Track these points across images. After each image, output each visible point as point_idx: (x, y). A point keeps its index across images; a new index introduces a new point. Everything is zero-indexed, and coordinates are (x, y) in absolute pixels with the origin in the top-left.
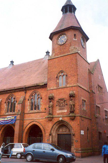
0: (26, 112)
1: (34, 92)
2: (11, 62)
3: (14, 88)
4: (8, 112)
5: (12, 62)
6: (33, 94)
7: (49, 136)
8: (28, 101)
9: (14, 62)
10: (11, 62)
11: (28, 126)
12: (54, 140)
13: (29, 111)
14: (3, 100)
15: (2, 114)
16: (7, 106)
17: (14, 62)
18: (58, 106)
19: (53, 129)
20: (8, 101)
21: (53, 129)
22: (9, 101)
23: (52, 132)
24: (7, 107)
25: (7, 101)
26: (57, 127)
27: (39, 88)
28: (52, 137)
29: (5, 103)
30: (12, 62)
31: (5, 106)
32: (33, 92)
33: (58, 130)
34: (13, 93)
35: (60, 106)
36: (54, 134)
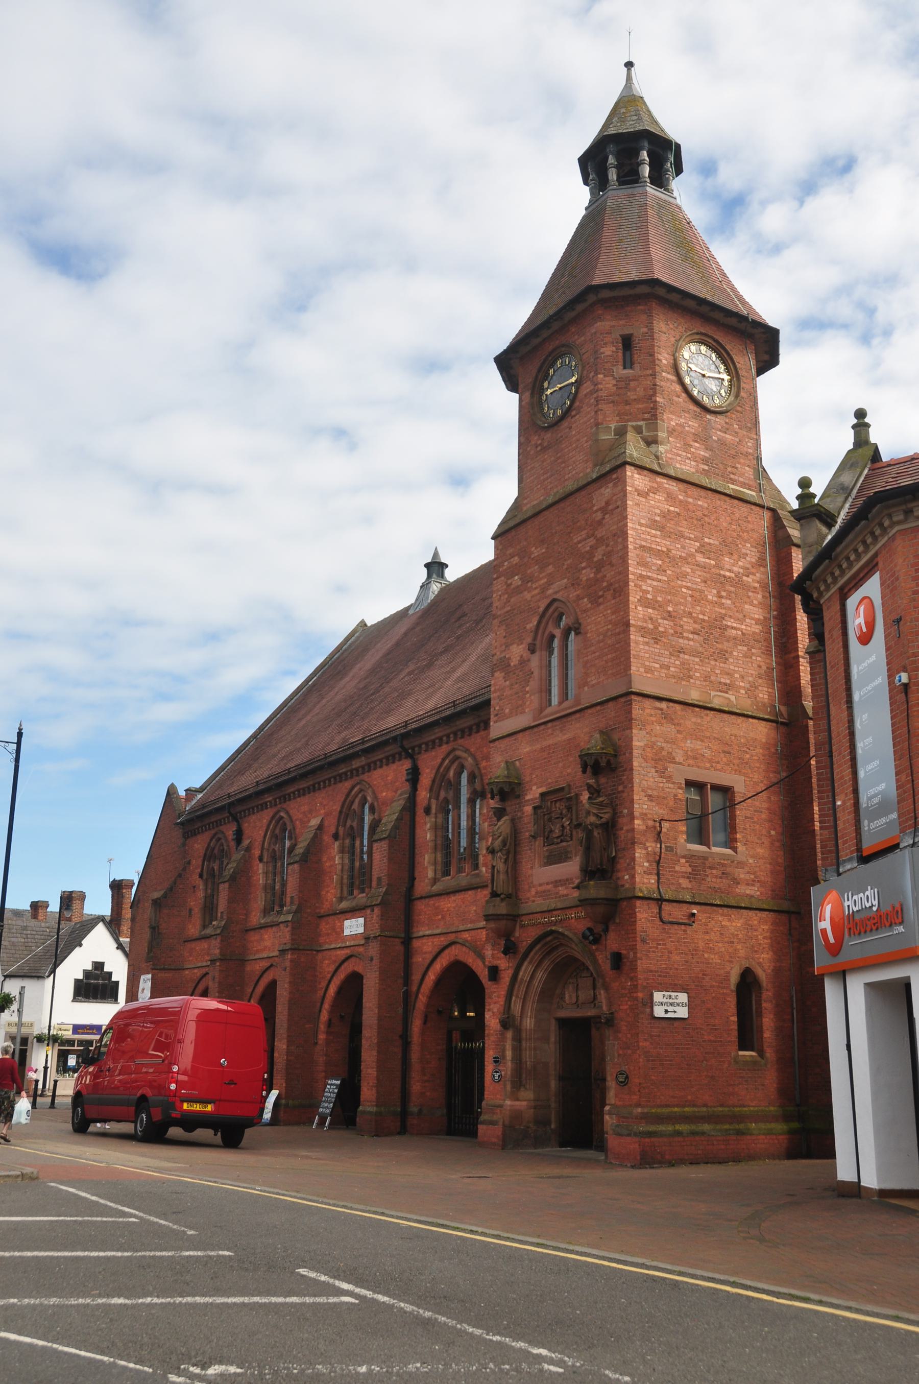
0: (422, 886)
1: (451, 757)
2: (427, 566)
3: (326, 758)
4: (446, 873)
5: (436, 568)
6: (352, 802)
7: (503, 1034)
8: (427, 819)
9: (447, 566)
10: (427, 566)
11: (432, 977)
12: (528, 1058)
13: (435, 881)
14: (326, 823)
15: (325, 907)
16: (346, 856)
17: (447, 566)
18: (540, 841)
19: (523, 988)
20: (349, 823)
21: (520, 990)
22: (352, 827)
23: (516, 1007)
24: (346, 861)
25: (344, 826)
26: (540, 975)
27: (470, 728)
28: (518, 1039)
29: (336, 837)
30: (436, 567)
31: (337, 860)
32: (444, 760)
33: (548, 995)
34: (365, 777)
35: (548, 840)
36: (528, 1023)
